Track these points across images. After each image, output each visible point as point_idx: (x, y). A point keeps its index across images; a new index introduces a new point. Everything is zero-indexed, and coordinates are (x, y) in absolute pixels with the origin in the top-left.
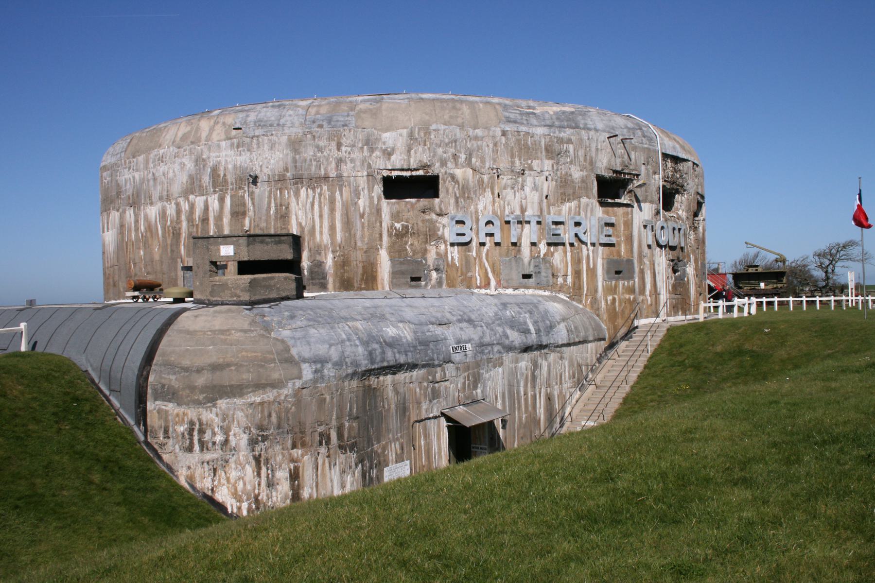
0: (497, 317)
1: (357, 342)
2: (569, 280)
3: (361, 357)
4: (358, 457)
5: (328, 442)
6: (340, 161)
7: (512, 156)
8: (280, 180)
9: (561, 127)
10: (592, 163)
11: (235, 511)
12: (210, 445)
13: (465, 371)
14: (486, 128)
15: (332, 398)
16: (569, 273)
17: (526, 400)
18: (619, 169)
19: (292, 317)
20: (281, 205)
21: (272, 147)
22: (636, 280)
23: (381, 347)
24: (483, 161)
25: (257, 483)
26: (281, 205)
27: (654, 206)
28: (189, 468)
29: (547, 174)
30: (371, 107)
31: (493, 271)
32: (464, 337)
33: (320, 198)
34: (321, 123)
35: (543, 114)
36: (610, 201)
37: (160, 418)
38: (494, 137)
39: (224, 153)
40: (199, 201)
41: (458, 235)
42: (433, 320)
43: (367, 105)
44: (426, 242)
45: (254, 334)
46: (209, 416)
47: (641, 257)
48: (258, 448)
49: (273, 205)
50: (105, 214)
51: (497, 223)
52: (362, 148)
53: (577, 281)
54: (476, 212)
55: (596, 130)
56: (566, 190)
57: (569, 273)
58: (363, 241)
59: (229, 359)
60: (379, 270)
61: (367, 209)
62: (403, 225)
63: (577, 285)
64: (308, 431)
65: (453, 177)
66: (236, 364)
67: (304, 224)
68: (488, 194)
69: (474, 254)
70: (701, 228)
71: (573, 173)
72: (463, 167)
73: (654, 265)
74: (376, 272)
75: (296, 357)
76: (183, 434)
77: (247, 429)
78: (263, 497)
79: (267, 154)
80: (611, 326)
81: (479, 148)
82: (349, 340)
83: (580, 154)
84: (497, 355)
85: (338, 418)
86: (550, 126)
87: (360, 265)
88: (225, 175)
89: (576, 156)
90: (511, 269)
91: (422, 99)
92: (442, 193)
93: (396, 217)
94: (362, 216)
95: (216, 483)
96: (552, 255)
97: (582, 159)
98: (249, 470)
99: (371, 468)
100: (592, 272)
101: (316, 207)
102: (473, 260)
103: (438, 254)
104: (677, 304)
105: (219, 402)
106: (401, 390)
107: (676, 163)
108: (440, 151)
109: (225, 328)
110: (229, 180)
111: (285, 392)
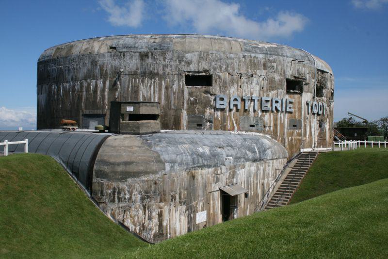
0: (242, 145)
1: (188, 154)
2: (272, 128)
3: (190, 161)
4: (187, 207)
5: (175, 200)
6: (165, 66)
7: (247, 68)
8: (134, 74)
9: (271, 54)
10: (284, 73)
11: (133, 230)
12: (123, 199)
13: (229, 170)
14: (236, 54)
15: (178, 180)
16: (272, 125)
17: (254, 185)
18: (297, 76)
19: (160, 141)
20: (135, 86)
21: (131, 57)
22: (303, 130)
23: (197, 157)
24: (233, 70)
25: (144, 218)
26: (135, 86)
27: (313, 94)
28: (113, 210)
29: (263, 77)
30: (181, 41)
31: (236, 123)
32: (230, 154)
33: (154, 84)
34: (156, 47)
35: (262, 48)
36: (292, 91)
37: (98, 186)
38: (239, 58)
39: (107, 59)
40: (93, 82)
41: (220, 104)
42: (217, 145)
43: (179, 40)
44: (205, 108)
45: (144, 148)
46: (123, 186)
47: (306, 118)
48: (145, 201)
49: (130, 86)
50: (40, 86)
51: (239, 100)
52: (176, 60)
53: (275, 129)
54: (229, 94)
55: (287, 57)
56: (272, 85)
57: (272, 125)
58: (174, 106)
59: (133, 159)
60: (182, 119)
61: (177, 90)
62: (194, 99)
63: (275, 131)
64: (167, 194)
65: (219, 77)
66: (137, 162)
67: (146, 96)
68: (235, 85)
69: (228, 115)
70: (332, 106)
71: (275, 77)
72: (224, 72)
73: (311, 123)
74: (180, 121)
75: (163, 160)
76: (110, 193)
77: (140, 192)
78: (146, 224)
79: (128, 61)
80: (290, 151)
81: (232, 63)
82: (185, 153)
83: (279, 68)
84: (243, 163)
85: (179, 189)
86: (266, 54)
87: (173, 117)
88: (106, 70)
89: (277, 69)
90: (245, 122)
91: (205, 38)
92: (213, 85)
93: (191, 94)
94: (174, 93)
95: (125, 217)
96: (264, 116)
97: (280, 70)
98: (141, 211)
99: (191, 213)
100: (282, 126)
101: (152, 88)
102: (227, 117)
103: (210, 113)
104: (321, 142)
105: (128, 179)
106: (204, 177)
107: (323, 74)
108: (213, 64)
109: (130, 145)
110: (109, 73)
111: (158, 176)
